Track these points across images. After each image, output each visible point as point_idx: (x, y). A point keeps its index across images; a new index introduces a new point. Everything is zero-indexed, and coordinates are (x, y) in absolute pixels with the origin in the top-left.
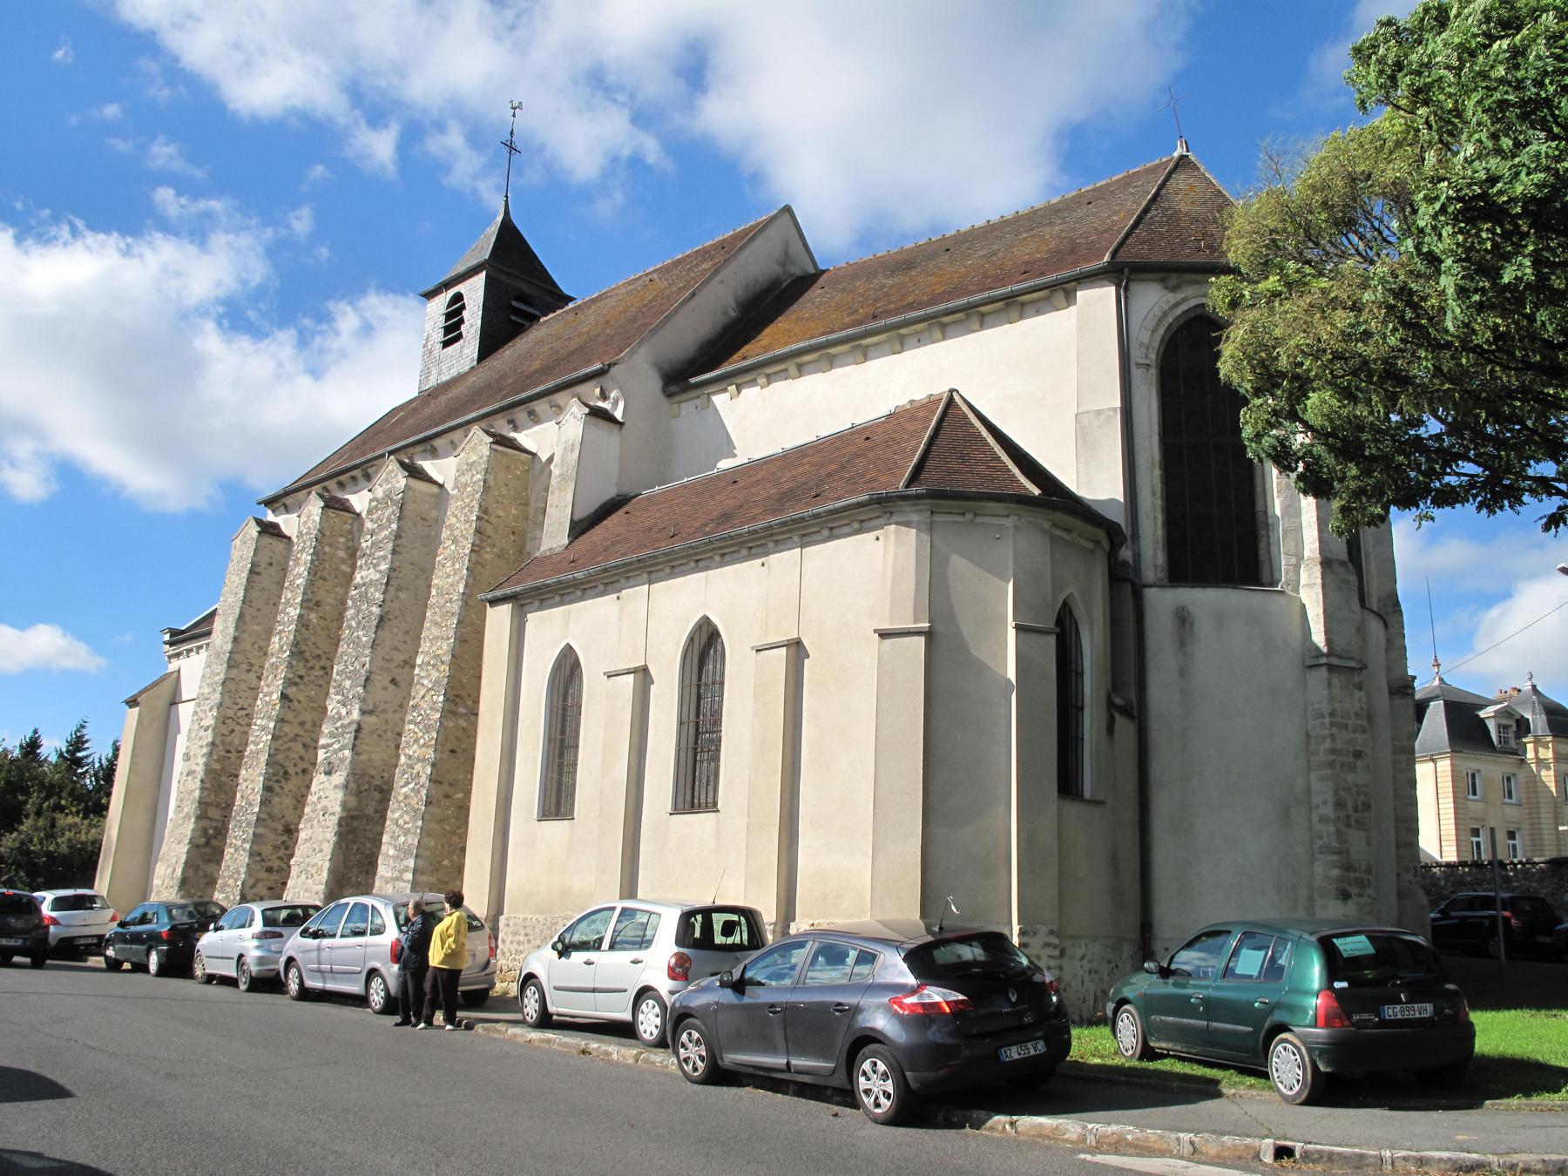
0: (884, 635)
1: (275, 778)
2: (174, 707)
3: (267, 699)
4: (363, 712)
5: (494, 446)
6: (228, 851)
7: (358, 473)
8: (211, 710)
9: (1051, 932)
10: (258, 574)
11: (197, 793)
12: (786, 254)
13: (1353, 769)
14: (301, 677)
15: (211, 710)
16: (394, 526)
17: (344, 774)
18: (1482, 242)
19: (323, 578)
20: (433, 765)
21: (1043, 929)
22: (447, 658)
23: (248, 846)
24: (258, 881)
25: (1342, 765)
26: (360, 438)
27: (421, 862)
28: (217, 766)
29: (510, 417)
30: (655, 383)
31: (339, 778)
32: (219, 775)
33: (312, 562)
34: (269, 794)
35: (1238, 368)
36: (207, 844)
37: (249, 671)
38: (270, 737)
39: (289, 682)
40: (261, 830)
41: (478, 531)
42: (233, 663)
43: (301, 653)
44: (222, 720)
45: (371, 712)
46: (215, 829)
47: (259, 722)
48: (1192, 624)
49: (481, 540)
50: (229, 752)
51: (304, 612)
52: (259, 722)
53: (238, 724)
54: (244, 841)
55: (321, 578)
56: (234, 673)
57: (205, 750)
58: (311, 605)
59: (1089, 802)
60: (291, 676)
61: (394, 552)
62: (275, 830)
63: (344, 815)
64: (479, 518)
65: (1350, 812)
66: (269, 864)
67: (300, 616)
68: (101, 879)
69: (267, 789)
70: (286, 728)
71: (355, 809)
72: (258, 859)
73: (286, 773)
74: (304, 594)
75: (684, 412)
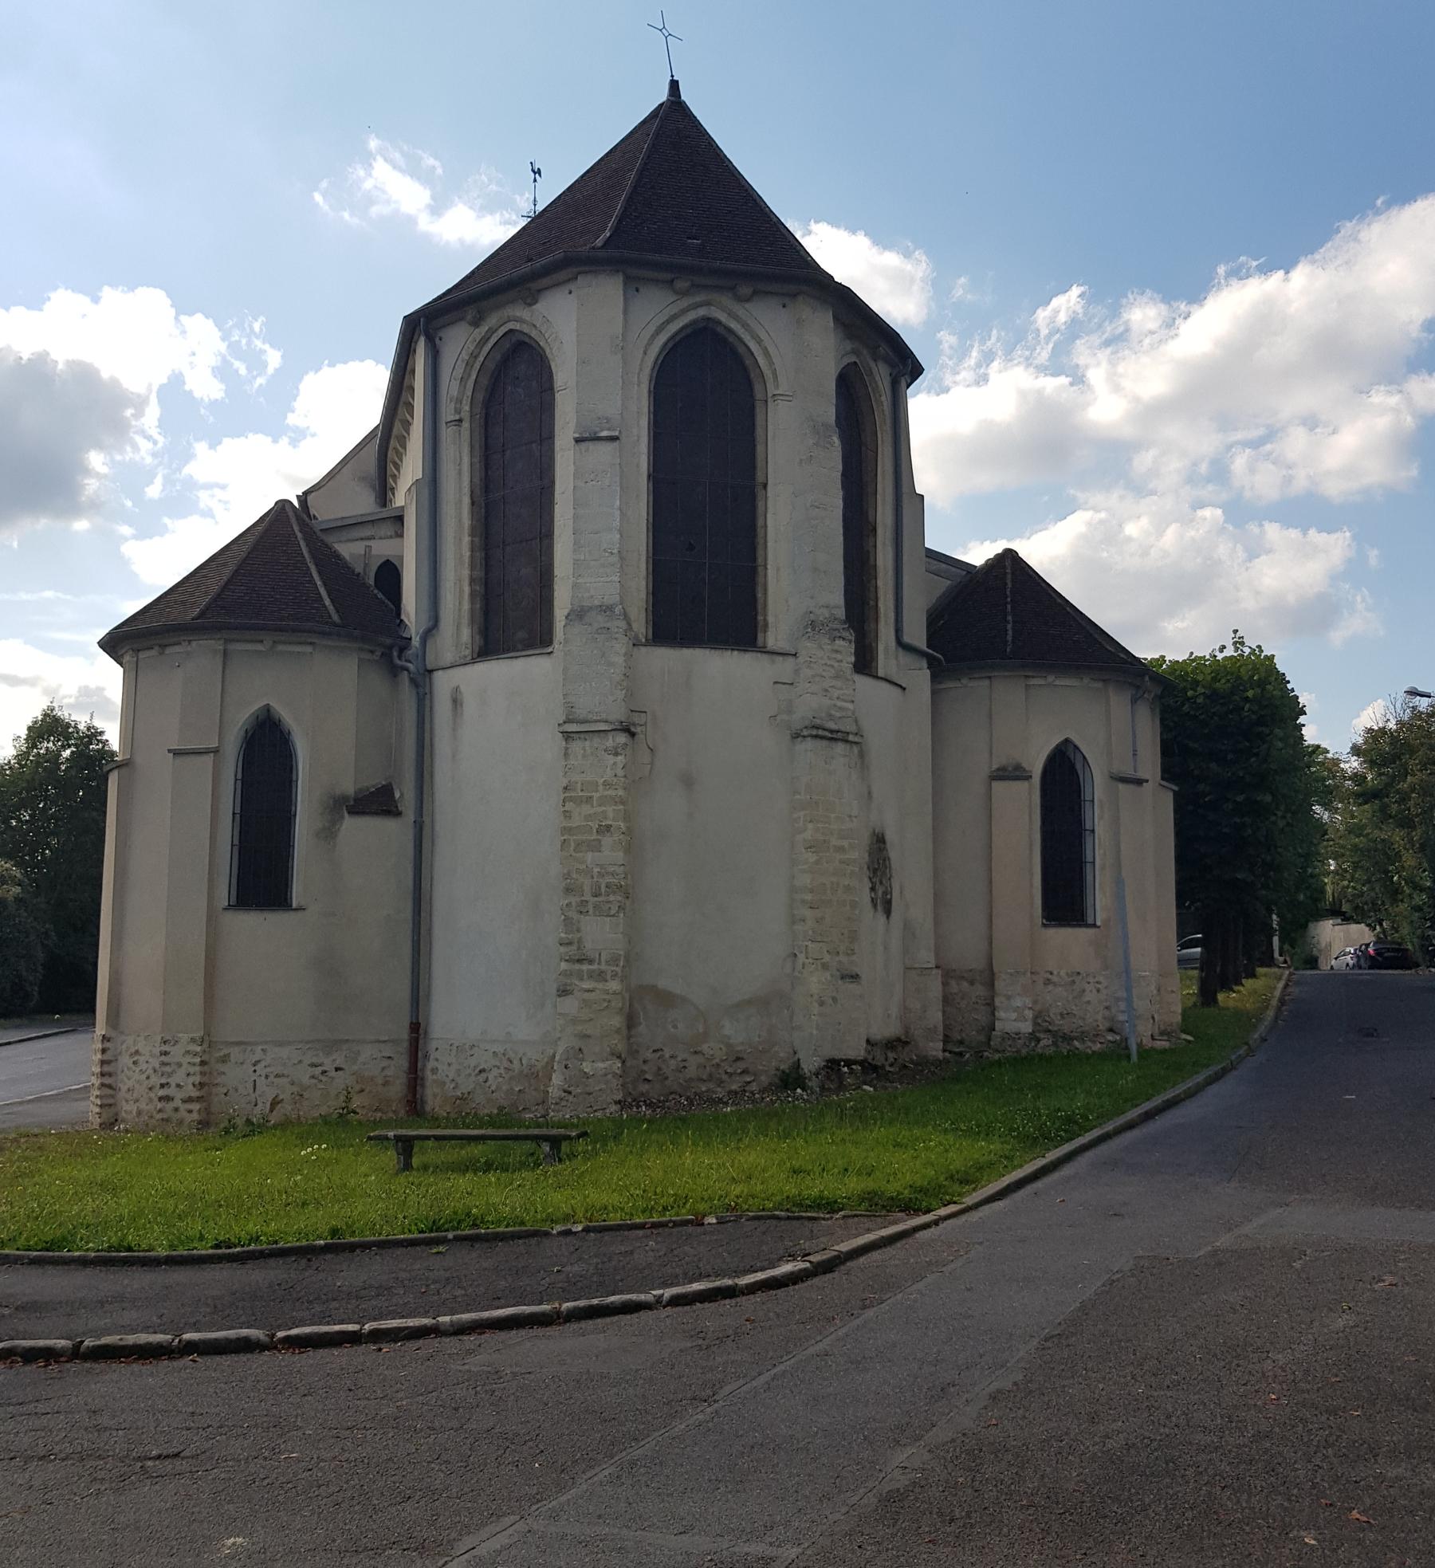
0: (177, 753)
9: (193, 1040)
13: (596, 847)
21: (184, 1037)
25: (578, 845)
29: (1400, 388)
35: (1044, 318)
48: (461, 705)
59: (296, 909)
65: (588, 897)
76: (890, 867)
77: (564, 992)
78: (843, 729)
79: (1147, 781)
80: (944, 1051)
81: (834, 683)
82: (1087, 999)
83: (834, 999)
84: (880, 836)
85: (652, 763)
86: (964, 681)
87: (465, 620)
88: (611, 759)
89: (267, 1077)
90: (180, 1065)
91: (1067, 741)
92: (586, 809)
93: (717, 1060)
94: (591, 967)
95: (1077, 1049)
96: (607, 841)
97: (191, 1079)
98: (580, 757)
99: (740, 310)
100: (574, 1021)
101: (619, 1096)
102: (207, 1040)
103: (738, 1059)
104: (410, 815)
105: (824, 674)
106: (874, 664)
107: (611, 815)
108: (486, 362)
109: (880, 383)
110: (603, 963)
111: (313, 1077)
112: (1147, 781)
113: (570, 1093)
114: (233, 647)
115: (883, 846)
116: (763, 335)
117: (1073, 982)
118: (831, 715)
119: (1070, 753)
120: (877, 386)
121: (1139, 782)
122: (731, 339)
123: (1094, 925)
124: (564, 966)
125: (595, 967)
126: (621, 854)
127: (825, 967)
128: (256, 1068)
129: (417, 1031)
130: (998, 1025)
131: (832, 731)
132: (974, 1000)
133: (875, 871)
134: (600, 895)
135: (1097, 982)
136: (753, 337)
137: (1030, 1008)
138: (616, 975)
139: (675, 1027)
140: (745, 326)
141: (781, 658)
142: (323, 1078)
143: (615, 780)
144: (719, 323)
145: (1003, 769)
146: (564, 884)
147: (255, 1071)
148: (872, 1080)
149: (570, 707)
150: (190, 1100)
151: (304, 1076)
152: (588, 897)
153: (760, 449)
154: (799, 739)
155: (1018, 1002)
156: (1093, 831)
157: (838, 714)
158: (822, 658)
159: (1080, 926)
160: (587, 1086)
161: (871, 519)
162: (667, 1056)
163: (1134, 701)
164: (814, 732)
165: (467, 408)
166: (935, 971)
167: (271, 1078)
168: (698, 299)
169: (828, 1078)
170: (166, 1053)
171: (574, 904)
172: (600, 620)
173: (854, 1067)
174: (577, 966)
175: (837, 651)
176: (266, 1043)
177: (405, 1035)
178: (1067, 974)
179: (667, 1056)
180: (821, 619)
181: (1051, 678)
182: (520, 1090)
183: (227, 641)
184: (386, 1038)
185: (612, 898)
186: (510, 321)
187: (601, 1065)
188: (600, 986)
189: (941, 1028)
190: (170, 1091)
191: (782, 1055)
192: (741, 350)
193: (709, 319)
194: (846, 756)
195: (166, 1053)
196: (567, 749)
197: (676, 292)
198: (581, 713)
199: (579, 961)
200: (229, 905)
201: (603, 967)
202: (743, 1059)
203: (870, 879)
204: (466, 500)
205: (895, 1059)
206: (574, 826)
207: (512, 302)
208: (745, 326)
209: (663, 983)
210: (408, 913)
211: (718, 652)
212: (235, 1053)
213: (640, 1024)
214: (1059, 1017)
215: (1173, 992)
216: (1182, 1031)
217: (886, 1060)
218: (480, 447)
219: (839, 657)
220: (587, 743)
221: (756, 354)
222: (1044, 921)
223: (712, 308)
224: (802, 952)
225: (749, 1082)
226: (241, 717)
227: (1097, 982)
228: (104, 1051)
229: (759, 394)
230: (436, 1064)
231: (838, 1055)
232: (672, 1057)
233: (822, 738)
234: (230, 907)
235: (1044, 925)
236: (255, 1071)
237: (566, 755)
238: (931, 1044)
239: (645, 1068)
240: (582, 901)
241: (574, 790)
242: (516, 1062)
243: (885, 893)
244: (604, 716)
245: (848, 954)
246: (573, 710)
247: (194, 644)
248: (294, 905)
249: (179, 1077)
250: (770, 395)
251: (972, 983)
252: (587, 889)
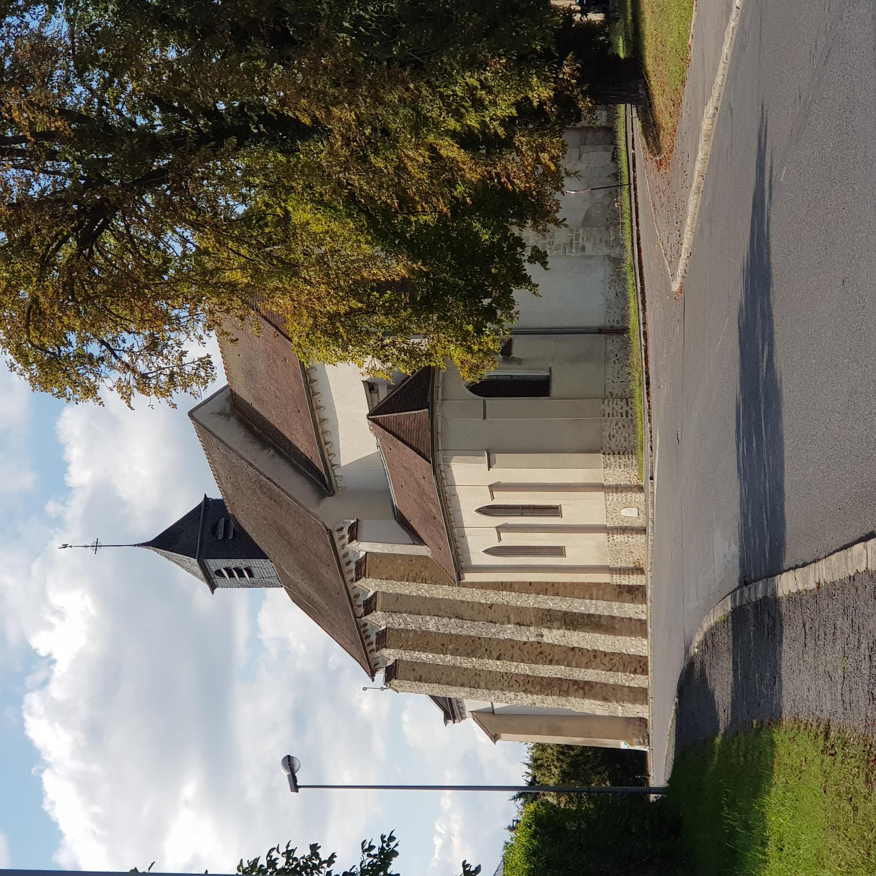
0: (485, 418)
1: (545, 659)
2: (496, 713)
3: (500, 667)
4: (509, 622)
5: (367, 576)
6: (586, 679)
7: (362, 630)
8: (505, 694)
9: (603, 403)
10: (421, 676)
11: (554, 697)
12: (220, 414)
14: (486, 650)
15: (505, 694)
16: (405, 615)
17: (543, 629)
18: (207, 66)
19: (428, 643)
20: (538, 594)
21: (602, 407)
22: (483, 591)
23: (583, 670)
24: (601, 663)
26: (320, 622)
27: (587, 596)
28: (538, 688)
30: (329, 501)
31: (545, 631)
32: (543, 685)
33: (419, 651)
34: (553, 661)
36: (583, 688)
37: (480, 676)
38: (522, 664)
39: (490, 657)
40: (574, 664)
41: (414, 581)
42: (476, 686)
43: (473, 651)
44: (510, 688)
45: (509, 618)
46: (574, 685)
47: (513, 670)
49: (419, 578)
50: (529, 681)
51: (449, 652)
52: (513, 670)
53: (511, 678)
54: (580, 672)
55: (428, 645)
56: (482, 684)
57: (529, 695)
58: (444, 649)
60: (486, 656)
61: (419, 614)
62: (574, 656)
63: (564, 627)
64: (407, 581)
66: (592, 657)
67: (451, 654)
68: (607, 745)
69: (551, 662)
70: (516, 655)
71: (561, 621)
72: (589, 663)
73: (541, 653)
74: (438, 653)
75: (343, 485)
90: (613, 408)
97: (619, 402)
100: (595, 244)
129: (601, 331)
130: (603, 125)
150: (627, 403)
170: (609, 415)
174: (574, 244)
188: (581, 236)
189: (605, 146)
190: (624, 411)
195: (609, 415)
199: (572, 244)
201: (574, 235)
209: (581, 219)
228: (609, 454)
230: (615, 322)
242: (613, 278)
248: (547, 374)
249: (618, 408)
252: (543, 242)
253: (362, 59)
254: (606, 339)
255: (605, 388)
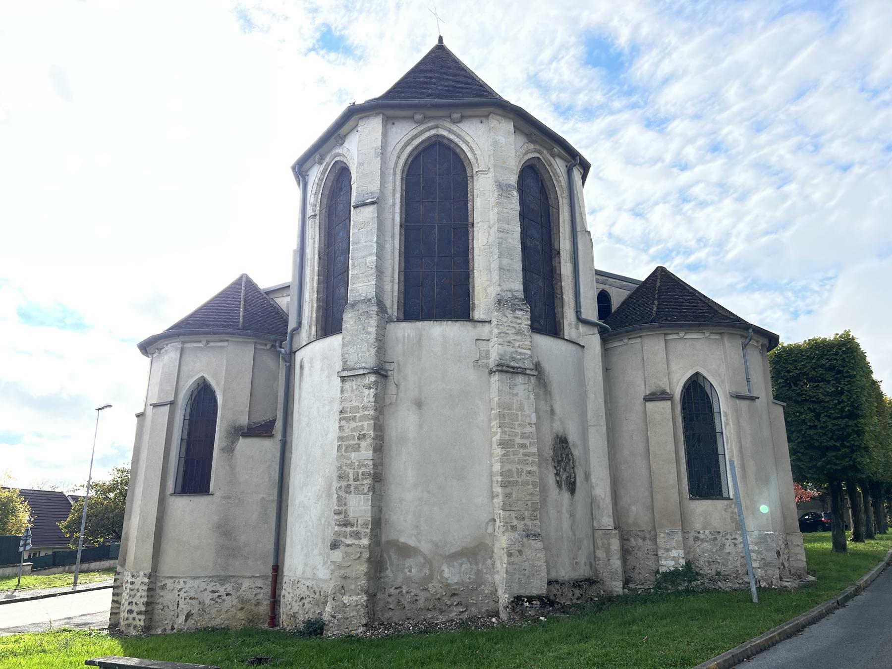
13: (356, 448)
21: (142, 573)
76: (573, 459)
77: (334, 546)
78: (523, 366)
79: (758, 398)
80: (624, 588)
81: (515, 337)
82: (728, 551)
83: (520, 552)
84: (563, 438)
85: (397, 394)
86: (626, 341)
87: (314, 323)
88: (366, 391)
89: (185, 599)
90: (138, 590)
91: (697, 374)
92: (353, 424)
93: (439, 596)
94: (351, 529)
95: (720, 588)
96: (363, 444)
98: (350, 392)
99: (455, 128)
100: (340, 567)
101: (364, 622)
102: (153, 575)
103: (454, 595)
104: (278, 436)
105: (508, 332)
106: (562, 333)
107: (366, 427)
108: (326, 182)
109: (558, 170)
110: (359, 526)
111: (212, 599)
112: (758, 398)
113: (335, 617)
114: (187, 345)
115: (565, 446)
116: (468, 138)
117: (716, 539)
118: (513, 358)
119: (701, 381)
120: (557, 172)
121: (753, 399)
122: (452, 145)
123: (729, 498)
124: (337, 528)
125: (354, 529)
126: (371, 452)
127: (514, 528)
128: (180, 593)
129: (277, 570)
131: (513, 368)
132: (646, 552)
133: (559, 462)
134: (358, 480)
135: (734, 539)
136: (464, 142)
137: (683, 558)
138: (367, 535)
139: (410, 571)
140: (459, 136)
141: (481, 324)
142: (219, 601)
143: (369, 404)
144: (444, 137)
145: (653, 394)
146: (338, 474)
147: (179, 595)
148: (549, 612)
149: (345, 361)
151: (207, 598)
152: (351, 482)
153: (470, 204)
154: (493, 374)
155: (674, 553)
156: (722, 433)
157: (519, 357)
158: (506, 322)
159: (718, 499)
160: (345, 613)
161: (556, 247)
162: (404, 592)
163: (744, 346)
164: (500, 368)
165: (318, 208)
166: (614, 532)
167: (188, 600)
168: (430, 124)
169: (513, 610)
171: (343, 487)
172: (363, 307)
173: (534, 602)
174: (344, 529)
175: (517, 318)
176: (186, 577)
177: (269, 572)
178: (711, 533)
179: (404, 592)
180: (505, 298)
181: (682, 334)
182: (319, 613)
183: (183, 342)
184: (258, 575)
185: (365, 482)
186: (336, 157)
187: (355, 598)
188: (356, 542)
191: (486, 592)
192: (458, 150)
193: (438, 135)
194: (525, 383)
196: (342, 387)
197: (416, 122)
198: (351, 364)
199: (345, 525)
200: (175, 493)
201: (359, 529)
202: (457, 595)
203: (555, 467)
204: (317, 257)
205: (582, 595)
206: (345, 435)
207: (334, 147)
208: (459, 136)
210: (275, 497)
211: (439, 322)
212: (169, 582)
213: (387, 569)
214: (707, 564)
215: (798, 546)
216: (809, 573)
217: (573, 595)
218: (325, 228)
219: (519, 321)
220: (354, 383)
221: (466, 151)
222: (691, 496)
223: (439, 129)
224: (498, 518)
225: (463, 612)
226: (189, 383)
227: (734, 539)
229: (469, 174)
231: (522, 592)
232: (408, 592)
233: (507, 372)
234: (175, 494)
235: (691, 498)
236: (179, 595)
237: (342, 391)
238: (614, 583)
239: (390, 600)
240: (348, 485)
241: (346, 412)
242: (318, 593)
243: (569, 477)
244: (363, 365)
245: (531, 519)
246: (347, 363)
247: (169, 346)
250: (474, 173)
251: (644, 539)
252: (351, 476)
253: (810, 475)
254: (264, 577)
255: (172, 577)
